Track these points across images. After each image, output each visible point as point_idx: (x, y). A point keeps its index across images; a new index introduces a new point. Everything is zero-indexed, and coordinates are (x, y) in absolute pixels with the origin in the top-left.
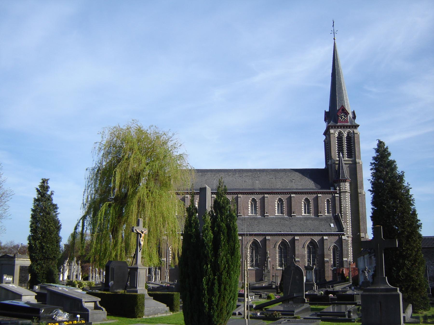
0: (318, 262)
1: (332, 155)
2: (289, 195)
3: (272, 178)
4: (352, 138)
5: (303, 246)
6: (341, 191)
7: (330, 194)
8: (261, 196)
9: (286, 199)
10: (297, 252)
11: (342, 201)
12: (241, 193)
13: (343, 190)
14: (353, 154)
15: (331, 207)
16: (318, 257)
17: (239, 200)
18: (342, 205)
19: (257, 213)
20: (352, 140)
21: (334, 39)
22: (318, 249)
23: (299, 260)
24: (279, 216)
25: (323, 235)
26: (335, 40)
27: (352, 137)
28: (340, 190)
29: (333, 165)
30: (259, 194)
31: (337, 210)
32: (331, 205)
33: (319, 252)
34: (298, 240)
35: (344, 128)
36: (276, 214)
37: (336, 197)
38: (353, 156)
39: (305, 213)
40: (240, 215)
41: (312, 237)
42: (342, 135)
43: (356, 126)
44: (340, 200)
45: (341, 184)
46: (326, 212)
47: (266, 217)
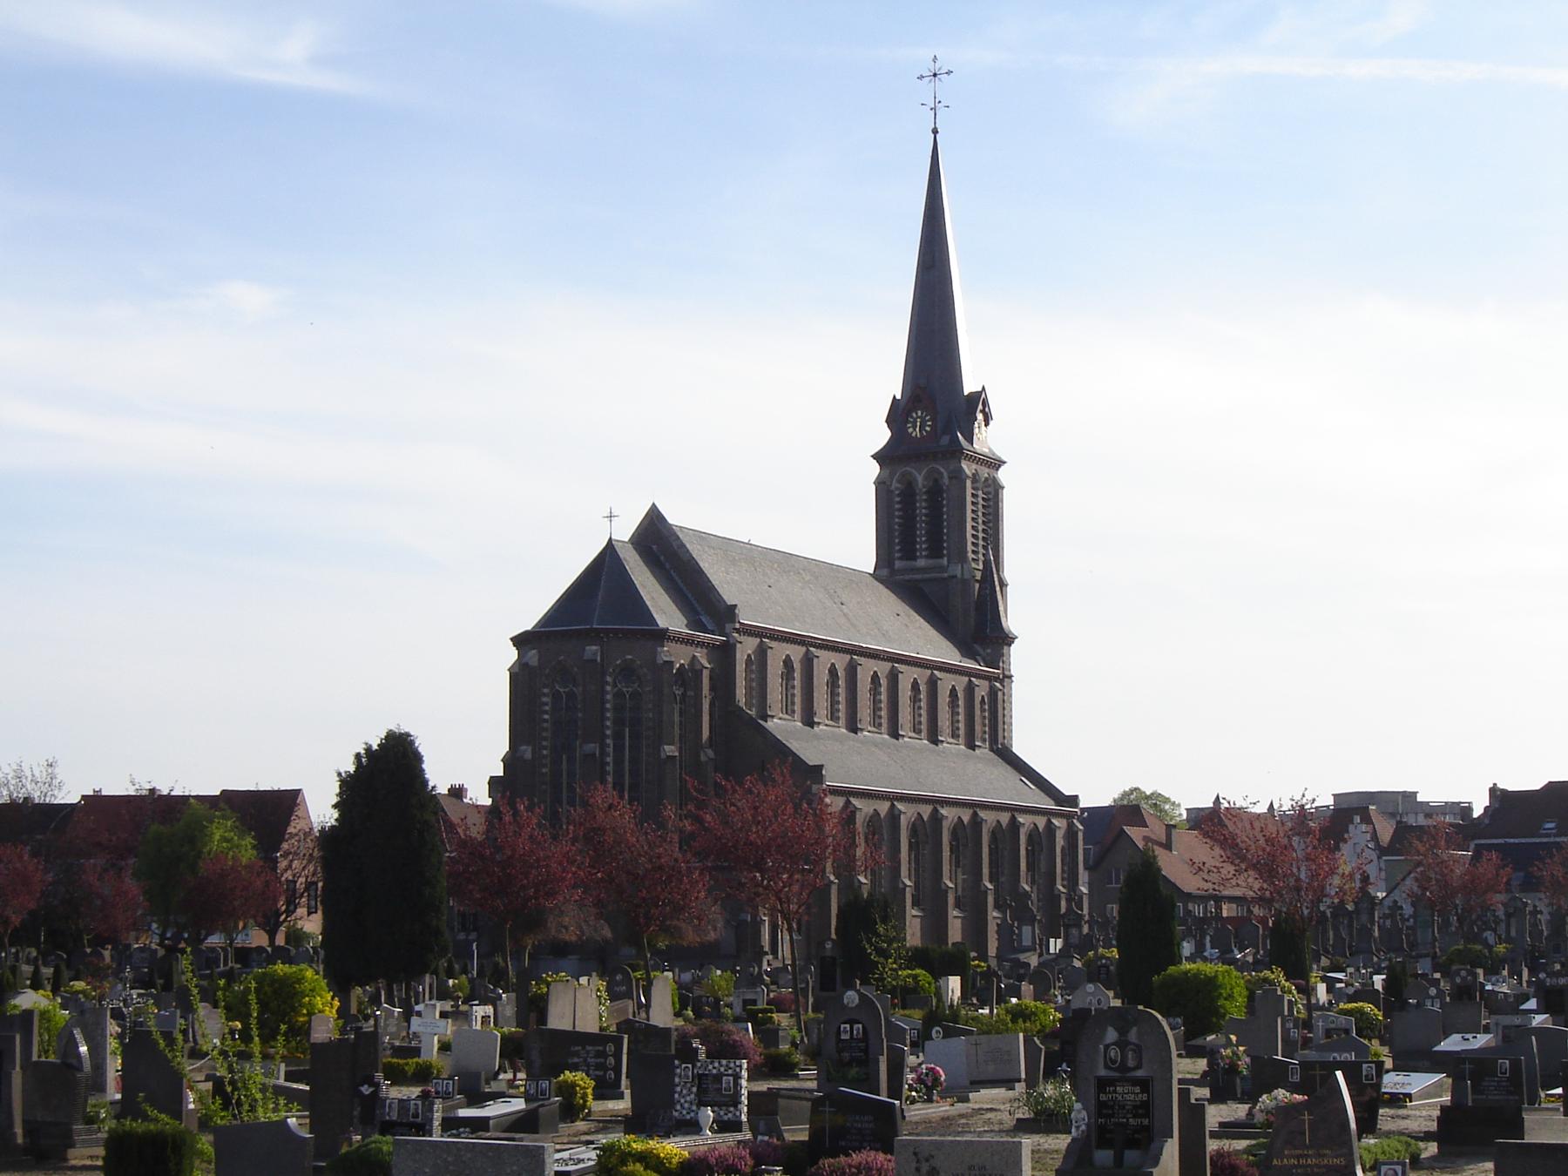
21: (935, 131)
26: (938, 136)
43: (996, 464)
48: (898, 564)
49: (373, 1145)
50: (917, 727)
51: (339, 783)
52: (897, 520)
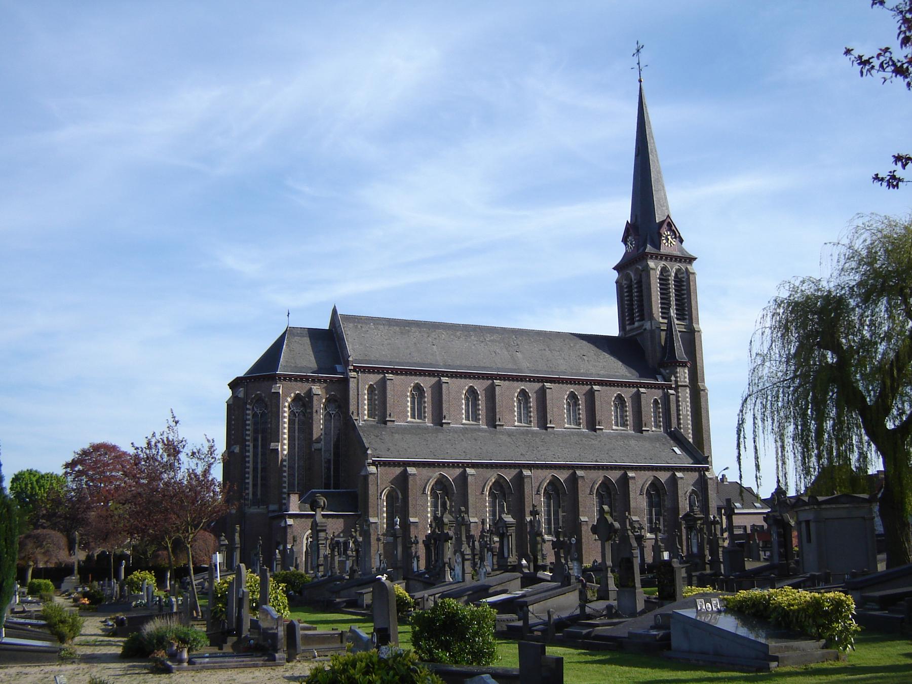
0: (666, 524)
1: (653, 312)
2: (589, 387)
3: (545, 350)
4: (683, 281)
5: (641, 492)
6: (679, 384)
7: (659, 388)
8: (537, 386)
9: (485, 390)
10: (633, 504)
11: (680, 404)
12: (395, 372)
13: (681, 382)
14: (687, 313)
15: (661, 415)
16: (666, 514)
17: (497, 393)
18: (681, 412)
19: (531, 421)
20: (684, 286)
21: (640, 81)
22: (666, 498)
23: (477, 521)
24: (466, 426)
25: (465, 466)
26: (642, 83)
27: (684, 279)
28: (676, 382)
29: (657, 331)
30: (534, 381)
31: (672, 421)
32: (661, 410)
33: (668, 503)
34: (633, 478)
35: (671, 260)
36: (409, 419)
37: (671, 396)
38: (687, 317)
39: (413, 416)
40: (499, 423)
41: (654, 472)
42: (666, 274)
43: (691, 260)
44: (678, 401)
45: (678, 370)
46: (409, 414)
47: (549, 430)
48: (628, 328)
49: (145, 672)
50: (578, 421)
51: (14, 476)
52: (626, 302)
